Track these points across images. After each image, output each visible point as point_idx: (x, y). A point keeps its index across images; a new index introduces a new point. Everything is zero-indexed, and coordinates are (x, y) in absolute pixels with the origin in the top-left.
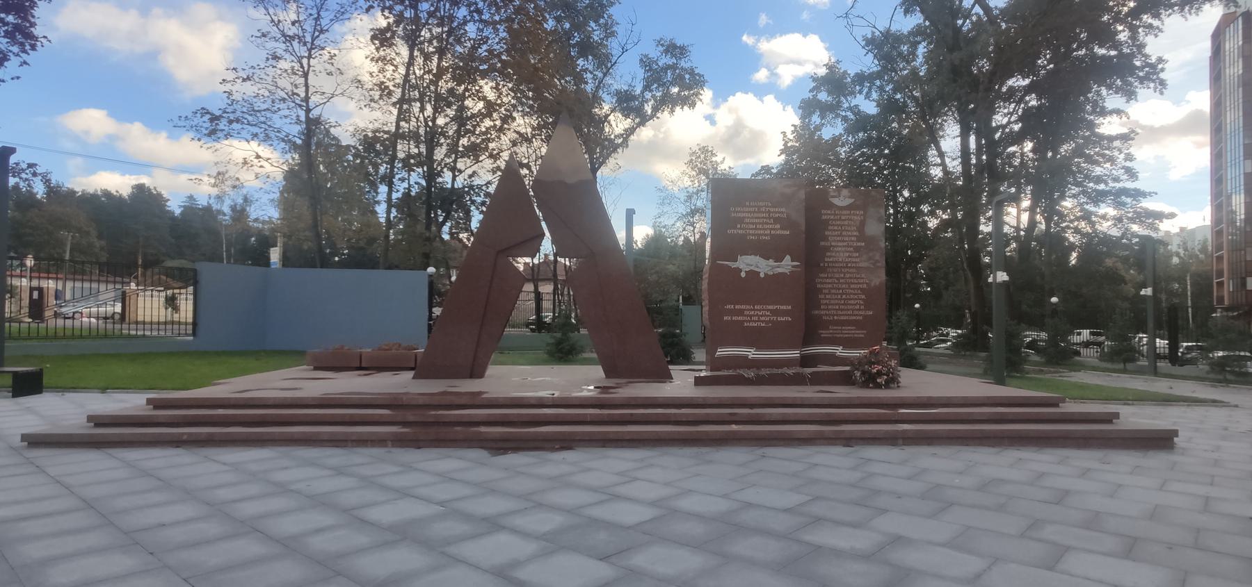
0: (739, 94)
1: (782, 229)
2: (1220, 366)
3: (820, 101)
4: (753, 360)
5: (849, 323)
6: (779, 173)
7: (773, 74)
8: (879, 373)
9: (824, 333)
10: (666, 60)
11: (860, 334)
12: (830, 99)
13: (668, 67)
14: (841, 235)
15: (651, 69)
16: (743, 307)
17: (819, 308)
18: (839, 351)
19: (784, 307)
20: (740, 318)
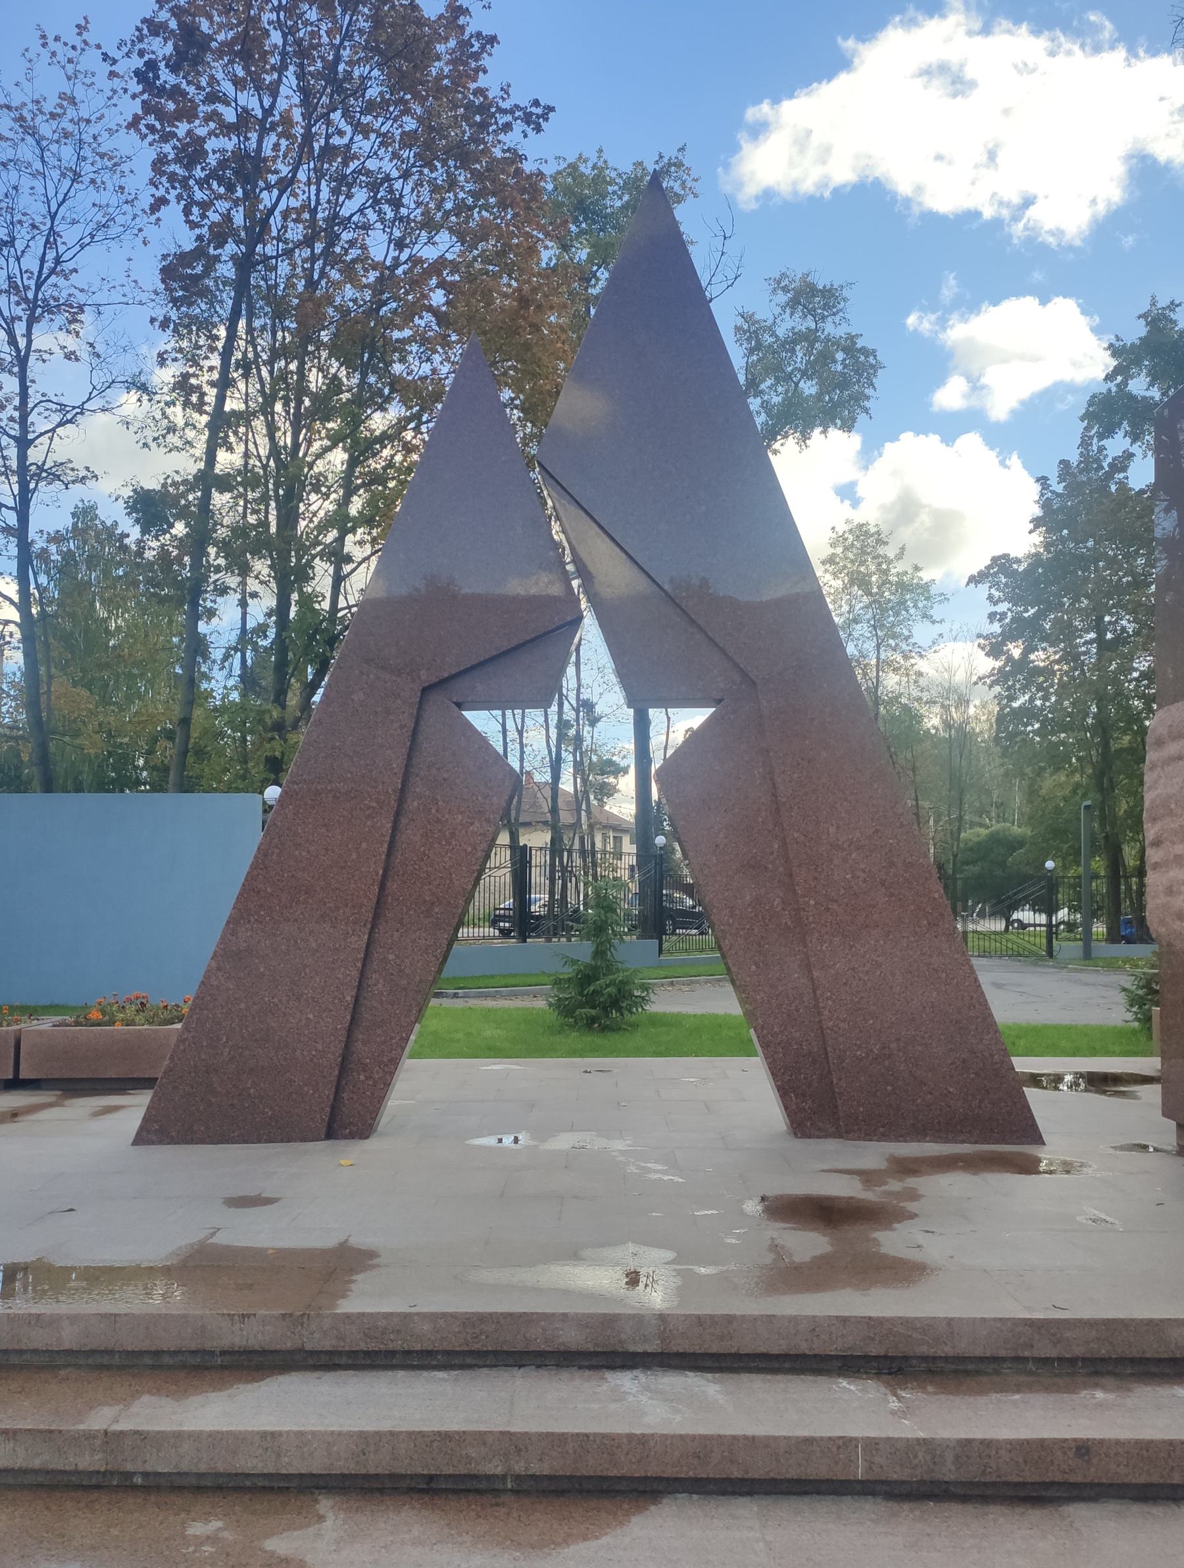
0: (907, 437)
2: (593, 1020)
3: (1132, 397)
6: (1030, 571)
7: (976, 386)
10: (788, 325)
12: (1155, 393)
13: (797, 338)
15: (759, 347)
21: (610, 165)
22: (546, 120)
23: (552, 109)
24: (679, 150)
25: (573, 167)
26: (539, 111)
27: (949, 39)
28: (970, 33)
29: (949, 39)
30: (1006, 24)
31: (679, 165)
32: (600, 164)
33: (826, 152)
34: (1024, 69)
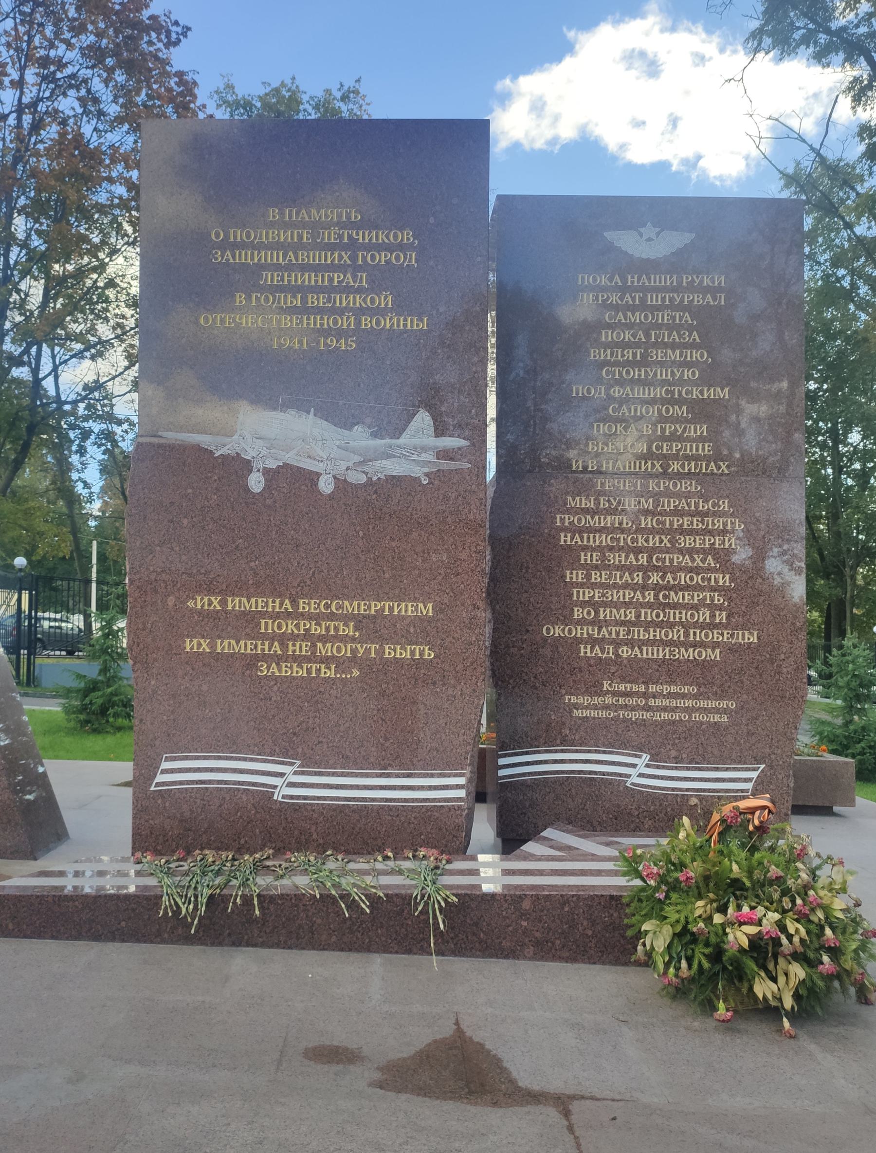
1: (400, 308)
4: (295, 810)
5: (670, 671)
8: (763, 951)
9: (584, 706)
11: (715, 711)
14: (644, 362)
16: (256, 604)
17: (567, 620)
18: (638, 771)
19: (406, 609)
20: (245, 647)
21: (301, 89)
22: (186, 36)
23: (189, 29)
24: (356, 81)
25: (277, 90)
26: (179, 30)
27: (647, 34)
28: (662, 31)
29: (647, 34)
30: (686, 23)
31: (357, 92)
32: (294, 88)
33: (556, 118)
34: (700, 59)
